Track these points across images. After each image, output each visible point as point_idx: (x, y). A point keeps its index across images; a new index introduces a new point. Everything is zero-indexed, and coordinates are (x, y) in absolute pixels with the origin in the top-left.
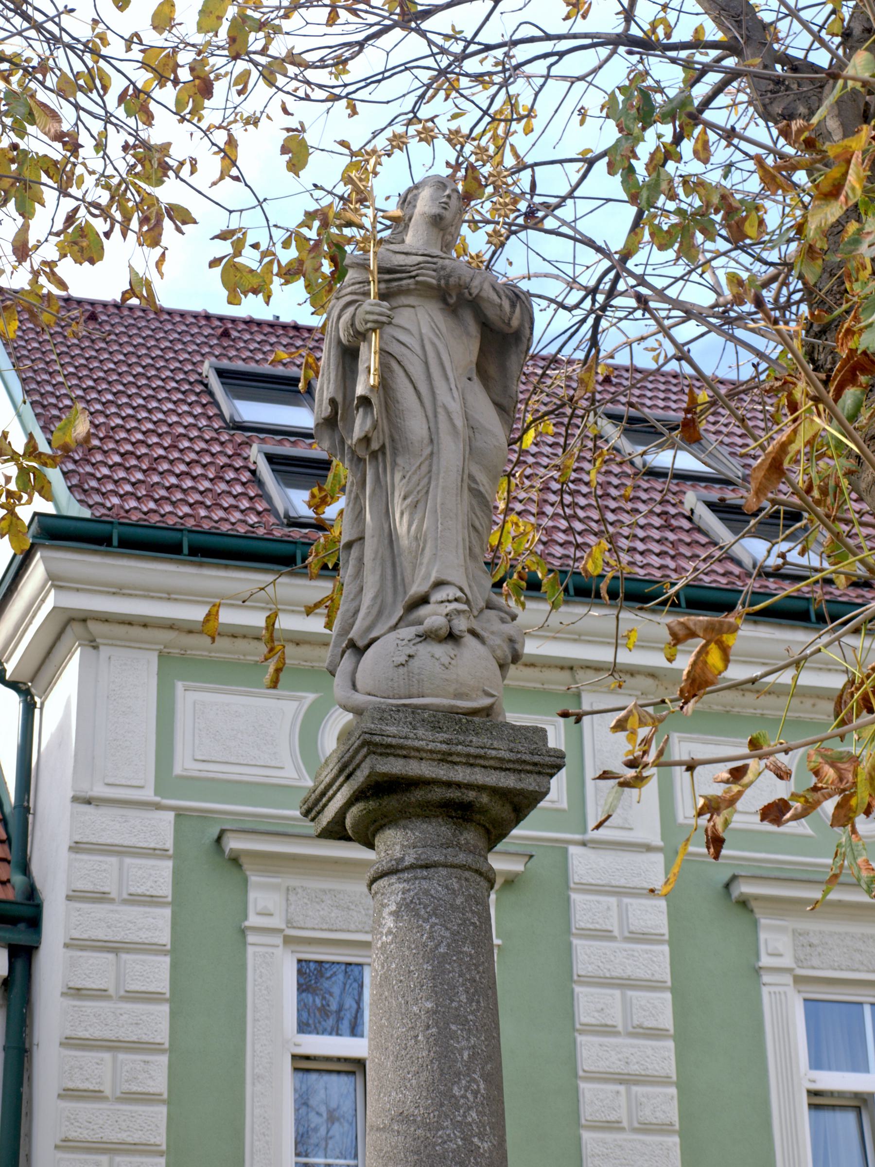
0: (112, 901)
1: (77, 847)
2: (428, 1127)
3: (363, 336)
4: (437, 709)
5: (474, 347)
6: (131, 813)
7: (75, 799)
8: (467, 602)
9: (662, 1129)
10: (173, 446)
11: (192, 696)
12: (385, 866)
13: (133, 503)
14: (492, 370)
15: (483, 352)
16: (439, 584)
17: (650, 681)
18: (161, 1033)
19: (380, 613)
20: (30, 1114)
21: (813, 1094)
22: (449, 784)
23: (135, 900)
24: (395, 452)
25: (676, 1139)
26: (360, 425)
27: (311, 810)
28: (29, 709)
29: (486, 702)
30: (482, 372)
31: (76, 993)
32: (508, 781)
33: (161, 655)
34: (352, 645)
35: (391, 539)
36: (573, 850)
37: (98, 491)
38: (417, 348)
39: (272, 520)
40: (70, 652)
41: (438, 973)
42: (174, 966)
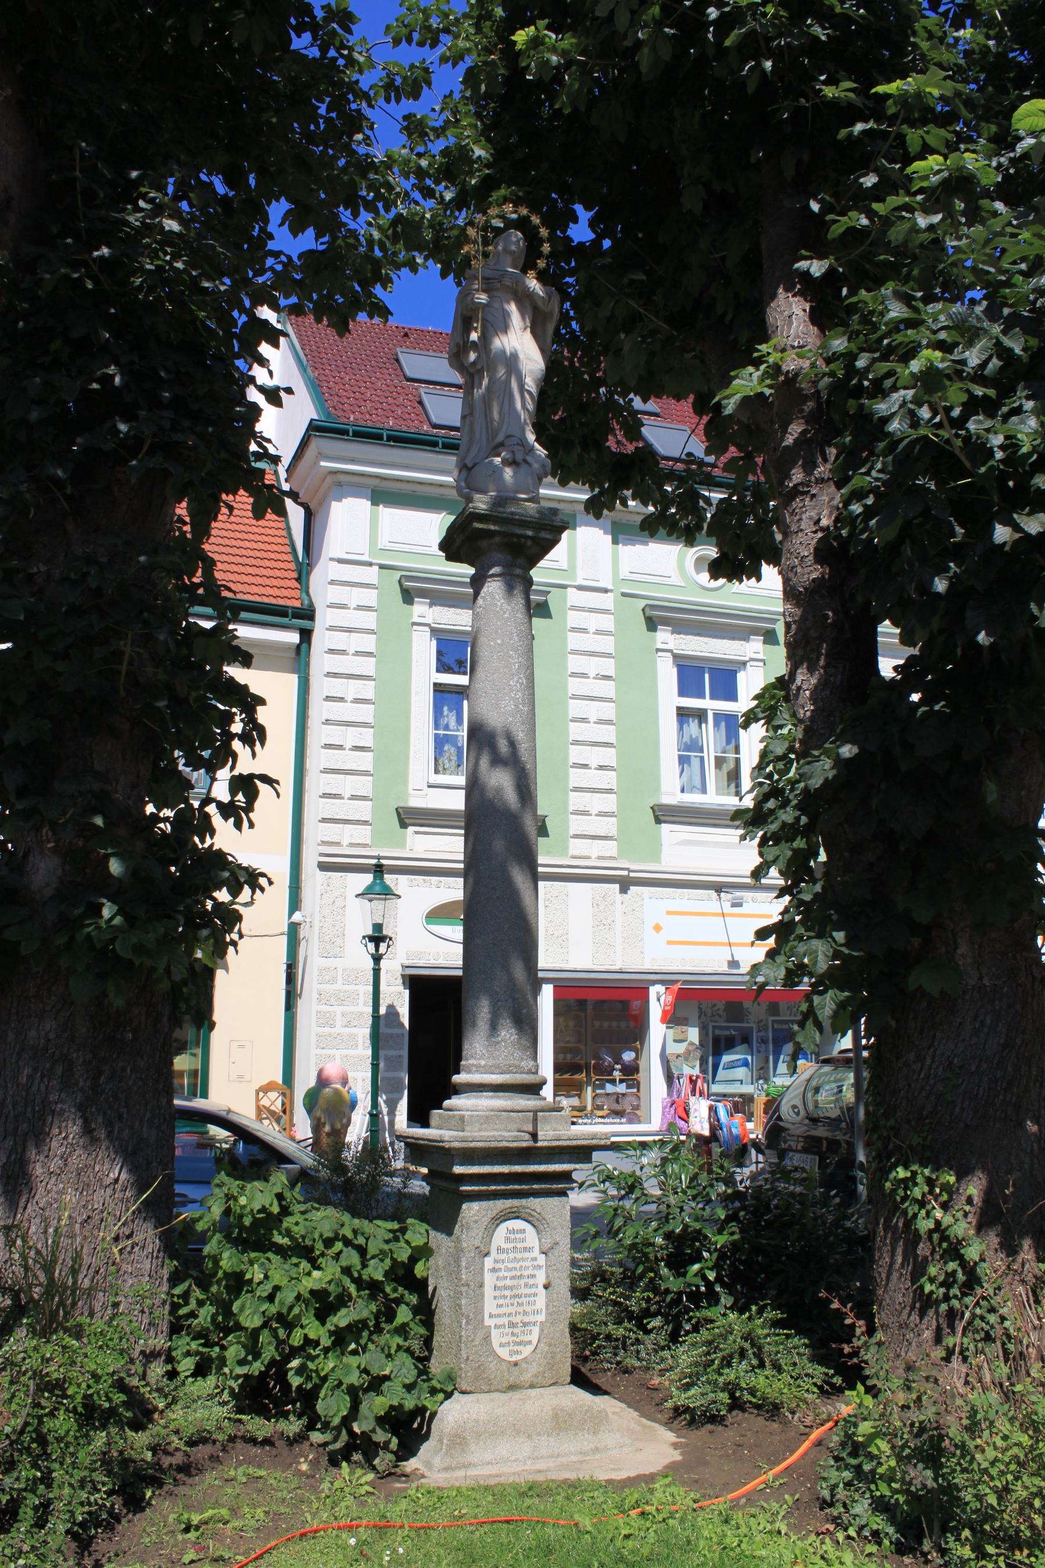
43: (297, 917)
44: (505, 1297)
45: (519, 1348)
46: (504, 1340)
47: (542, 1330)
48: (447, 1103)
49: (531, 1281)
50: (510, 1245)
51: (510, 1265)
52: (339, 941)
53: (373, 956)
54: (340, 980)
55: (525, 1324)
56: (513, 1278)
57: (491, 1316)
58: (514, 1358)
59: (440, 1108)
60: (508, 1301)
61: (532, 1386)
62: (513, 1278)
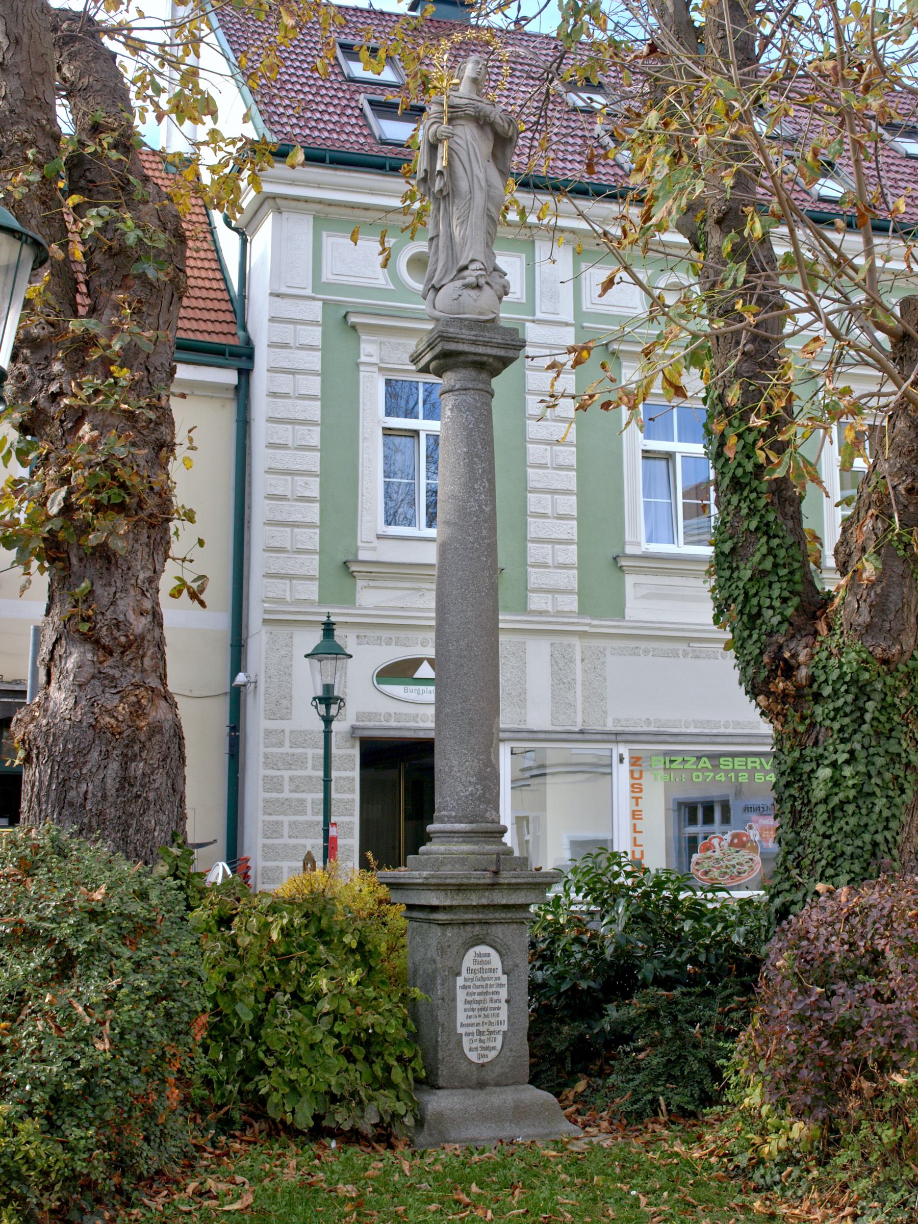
0: (291, 348)
1: (272, 320)
2: (464, 501)
3: (441, 141)
4: (470, 320)
5: (491, 145)
6: (300, 302)
7: (271, 294)
8: (485, 270)
9: (568, 468)
10: (317, 93)
11: (331, 240)
12: (447, 388)
13: (297, 131)
14: (499, 155)
15: (495, 146)
16: (473, 261)
17: (571, 235)
18: (317, 416)
19: (446, 272)
20: (250, 454)
21: (644, 451)
22: (475, 354)
23: (303, 347)
24: (454, 197)
25: (575, 473)
26: (438, 184)
27: (414, 360)
28: (244, 242)
29: (492, 316)
30: (494, 156)
31: (274, 395)
32: (501, 353)
33: (315, 217)
34: (433, 287)
35: (451, 237)
36: (528, 324)
37: (279, 122)
38: (465, 147)
39: (372, 141)
40: (267, 214)
41: (469, 436)
42: (323, 382)
43: (241, 678)
44: (474, 1010)
45: (486, 1052)
46: (474, 1045)
47: (504, 1038)
48: (422, 849)
49: (495, 997)
50: (478, 967)
51: (478, 983)
52: (285, 702)
53: (323, 717)
54: (287, 743)
55: (490, 1033)
56: (480, 994)
57: (462, 1025)
58: (481, 1062)
59: (417, 853)
60: (476, 1013)
61: (497, 1085)
62: (480, 994)
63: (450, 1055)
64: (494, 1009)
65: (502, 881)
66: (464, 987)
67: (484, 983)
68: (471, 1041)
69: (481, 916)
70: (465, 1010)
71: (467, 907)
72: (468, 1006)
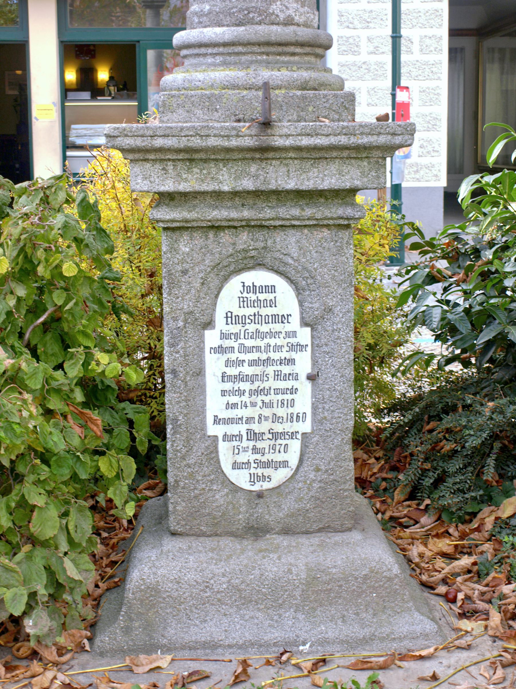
44: (241, 393)
45: (267, 472)
46: (243, 458)
50: (249, 311)
51: (249, 343)
55: (276, 436)
56: (253, 363)
57: (217, 421)
58: (257, 488)
60: (246, 398)
62: (253, 363)
63: (191, 475)
64: (284, 391)
65: (279, 142)
66: (220, 350)
67: (261, 343)
68: (236, 451)
69: (246, 214)
70: (224, 393)
71: (218, 195)
72: (228, 386)
